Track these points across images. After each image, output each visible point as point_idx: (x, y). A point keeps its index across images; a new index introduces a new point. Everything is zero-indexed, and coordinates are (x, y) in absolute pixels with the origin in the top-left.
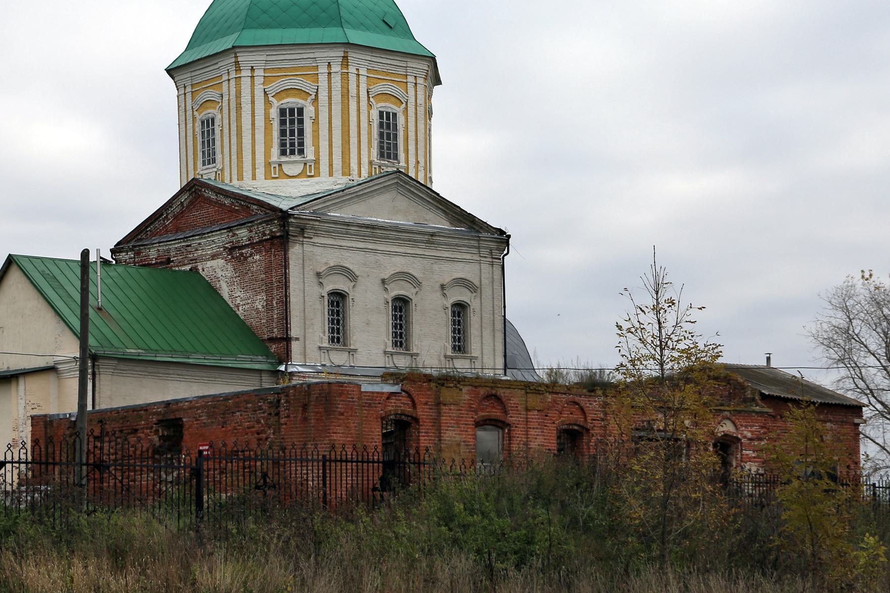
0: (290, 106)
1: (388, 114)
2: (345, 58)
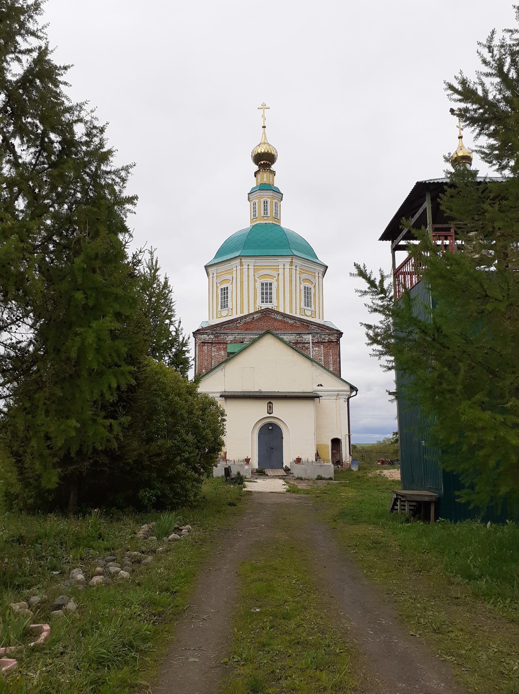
0: (266, 282)
1: (308, 288)
2: (241, 263)
